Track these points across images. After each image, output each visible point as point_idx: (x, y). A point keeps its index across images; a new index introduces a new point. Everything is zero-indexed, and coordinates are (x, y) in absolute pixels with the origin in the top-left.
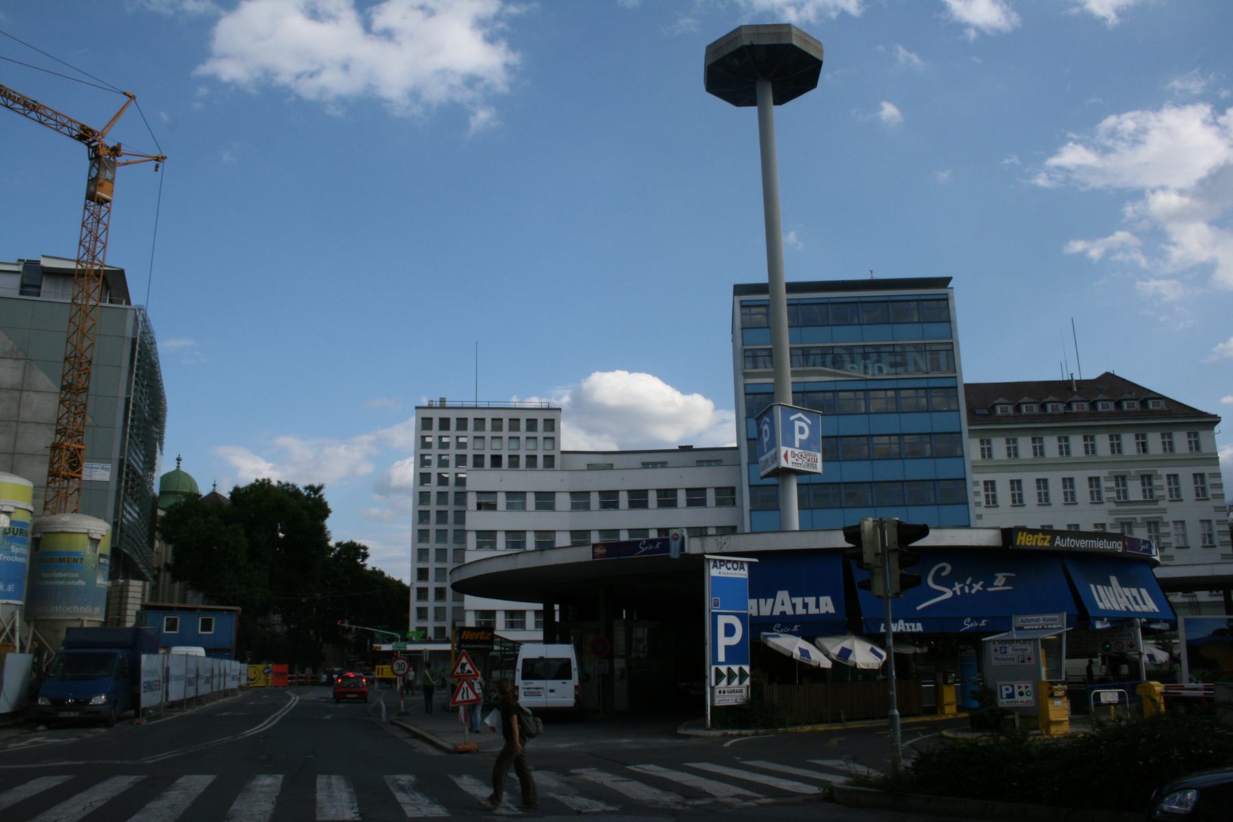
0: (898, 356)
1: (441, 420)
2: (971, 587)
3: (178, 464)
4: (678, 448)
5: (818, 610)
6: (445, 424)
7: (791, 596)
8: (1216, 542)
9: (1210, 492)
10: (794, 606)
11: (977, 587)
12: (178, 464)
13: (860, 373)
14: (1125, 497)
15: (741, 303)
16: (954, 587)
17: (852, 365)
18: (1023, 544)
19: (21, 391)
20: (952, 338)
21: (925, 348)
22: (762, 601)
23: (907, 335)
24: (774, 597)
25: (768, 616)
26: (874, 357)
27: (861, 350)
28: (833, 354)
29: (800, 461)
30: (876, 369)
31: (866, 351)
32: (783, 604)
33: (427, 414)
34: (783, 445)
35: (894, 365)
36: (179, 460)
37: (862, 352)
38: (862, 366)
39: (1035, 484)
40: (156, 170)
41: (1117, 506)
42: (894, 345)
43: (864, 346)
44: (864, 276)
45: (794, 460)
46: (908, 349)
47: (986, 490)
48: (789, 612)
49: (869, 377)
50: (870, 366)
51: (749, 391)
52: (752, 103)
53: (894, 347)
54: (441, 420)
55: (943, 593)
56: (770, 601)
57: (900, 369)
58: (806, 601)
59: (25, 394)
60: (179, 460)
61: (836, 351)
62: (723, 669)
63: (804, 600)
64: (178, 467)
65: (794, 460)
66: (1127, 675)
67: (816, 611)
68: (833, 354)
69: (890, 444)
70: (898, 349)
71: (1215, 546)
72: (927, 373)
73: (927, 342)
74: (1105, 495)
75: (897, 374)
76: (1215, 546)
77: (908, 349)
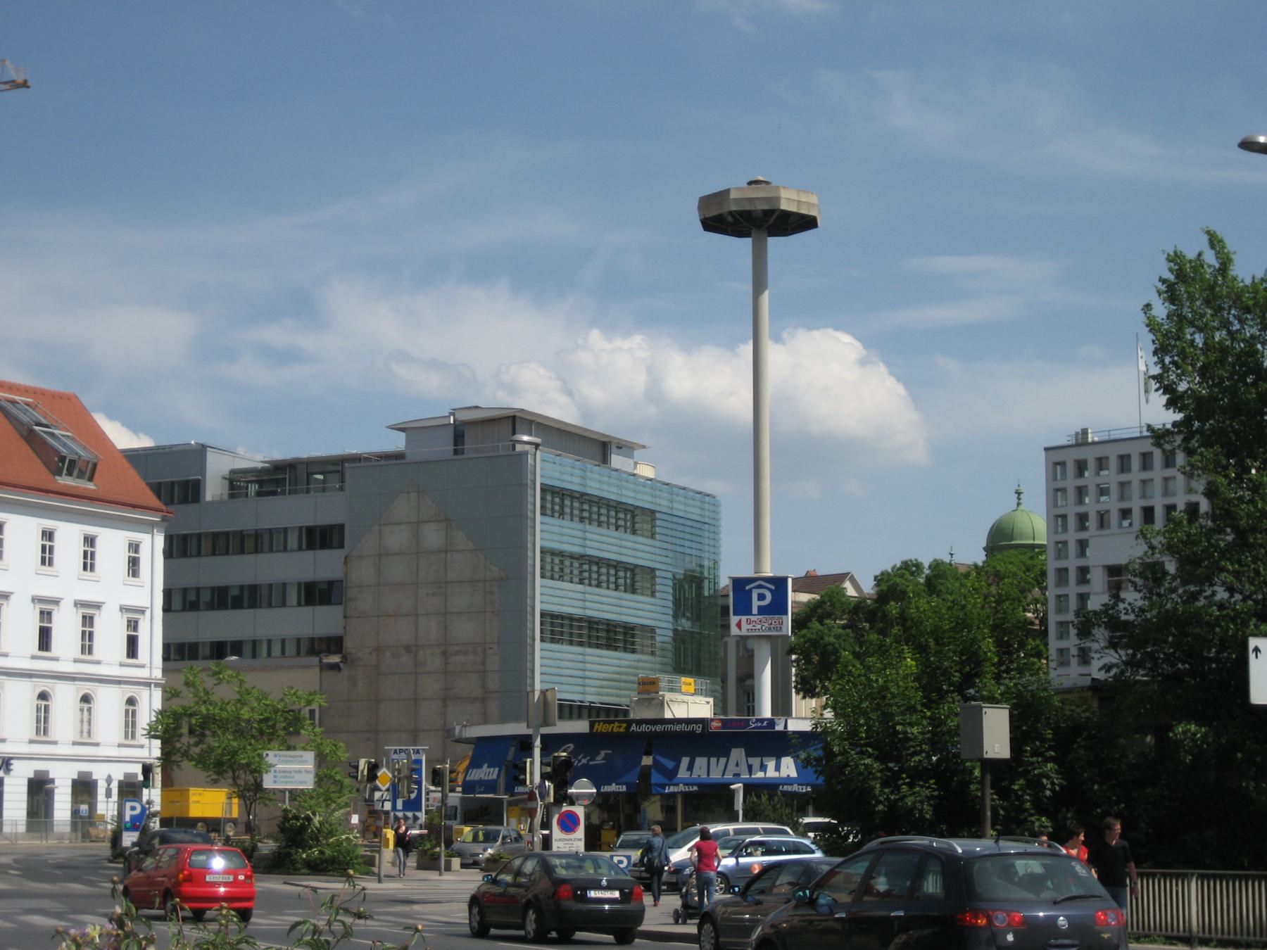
2: (580, 761)
6: (1081, 467)
7: (748, 755)
9: (940, 642)
19: (446, 552)
22: (713, 760)
24: (727, 755)
29: (759, 627)
32: (737, 765)
33: (1059, 456)
34: (734, 614)
40: (807, 223)
45: (750, 627)
55: (812, 852)
56: (723, 760)
58: (750, 763)
62: (400, 814)
65: (750, 627)
67: (776, 774)
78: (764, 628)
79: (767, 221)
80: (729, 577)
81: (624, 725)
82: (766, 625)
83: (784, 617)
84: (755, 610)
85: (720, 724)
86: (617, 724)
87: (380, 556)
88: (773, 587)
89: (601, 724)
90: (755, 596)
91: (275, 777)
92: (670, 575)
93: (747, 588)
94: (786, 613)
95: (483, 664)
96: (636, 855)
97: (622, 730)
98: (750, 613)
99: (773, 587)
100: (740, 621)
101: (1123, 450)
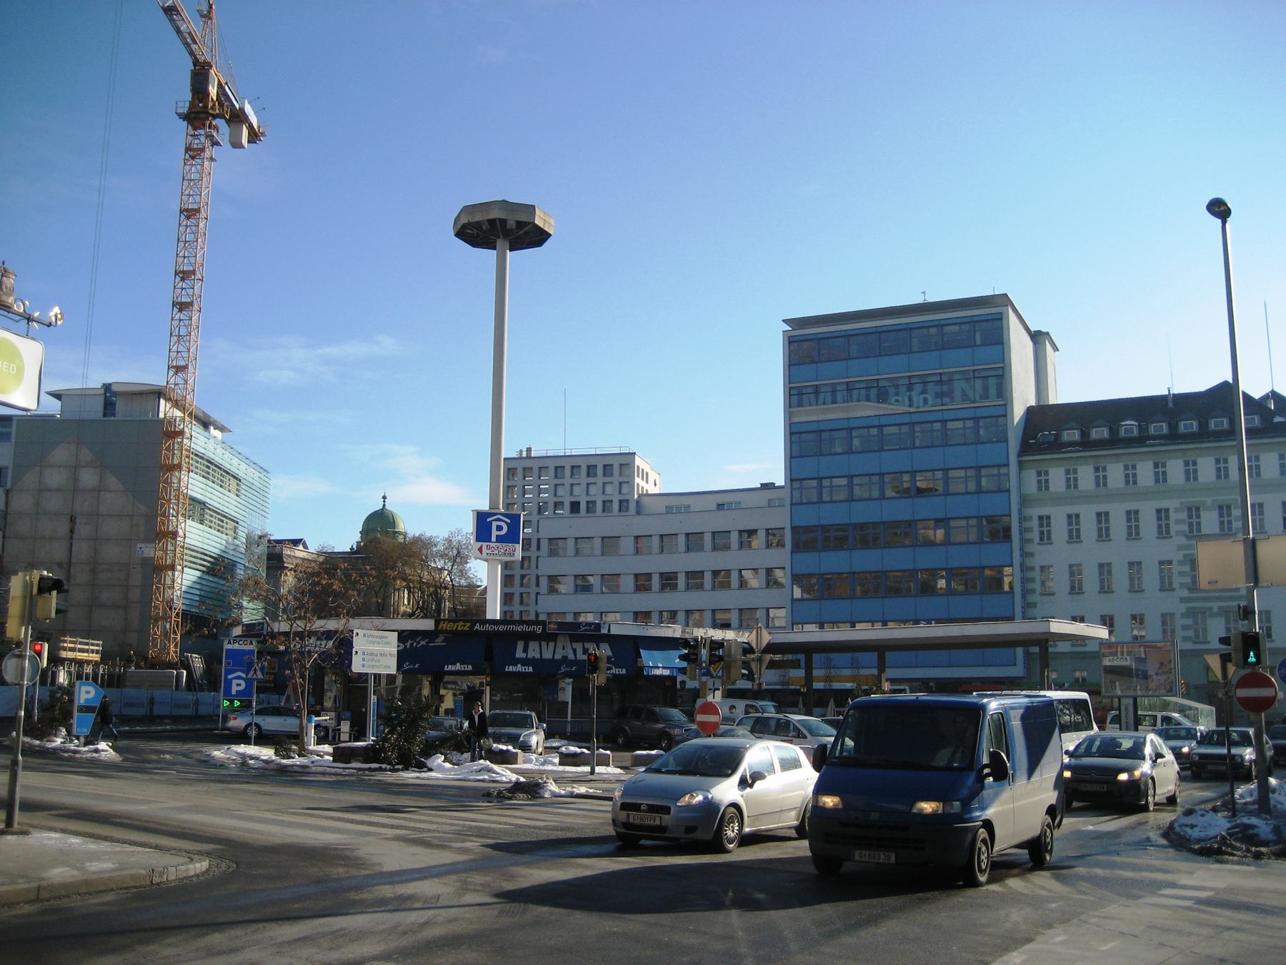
0: (944, 385)
1: (497, 530)
2: (418, 643)
3: (384, 502)
4: (759, 486)
5: (525, 654)
8: (1175, 585)
10: (575, 651)
11: (423, 643)
12: (384, 502)
13: (904, 406)
14: (1199, 530)
15: (789, 339)
16: (407, 642)
17: (897, 398)
18: (444, 628)
19: (99, 491)
20: (1004, 362)
21: (974, 375)
23: (956, 361)
25: (549, 660)
26: (918, 388)
27: (906, 381)
28: (877, 387)
30: (921, 400)
31: (912, 382)
35: (940, 395)
36: (384, 498)
37: (908, 383)
38: (906, 399)
39: (1094, 518)
41: (1187, 540)
42: (940, 374)
43: (909, 377)
44: (916, 299)
45: (489, 552)
46: (956, 377)
47: (1041, 525)
48: (571, 657)
49: (912, 410)
50: (915, 399)
51: (794, 430)
52: (494, 248)
53: (909, 379)
54: (497, 530)
57: (946, 400)
59: (102, 493)
60: (384, 498)
61: (882, 384)
63: (584, 647)
64: (384, 505)
65: (489, 552)
66: (557, 699)
68: (877, 387)
69: (934, 480)
70: (945, 378)
71: (1174, 590)
72: (974, 402)
73: (976, 368)
74: (1174, 528)
75: (942, 405)
76: (1174, 590)
77: (956, 377)
78: (500, 553)
79: (517, 233)
80: (473, 511)
81: (468, 624)
82: (502, 551)
83: (516, 545)
84: (494, 539)
85: (556, 626)
86: (461, 623)
87: (40, 491)
88: (509, 521)
89: (446, 622)
90: (494, 525)
91: (364, 660)
92: (246, 531)
93: (488, 520)
94: (519, 543)
95: (127, 580)
96: (534, 746)
97: (466, 628)
98: (490, 541)
99: (509, 521)
100: (482, 546)
101: (592, 461)
